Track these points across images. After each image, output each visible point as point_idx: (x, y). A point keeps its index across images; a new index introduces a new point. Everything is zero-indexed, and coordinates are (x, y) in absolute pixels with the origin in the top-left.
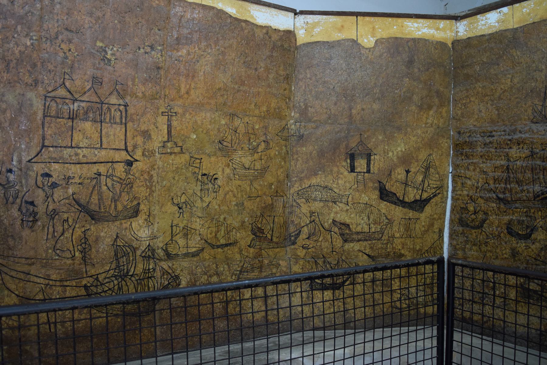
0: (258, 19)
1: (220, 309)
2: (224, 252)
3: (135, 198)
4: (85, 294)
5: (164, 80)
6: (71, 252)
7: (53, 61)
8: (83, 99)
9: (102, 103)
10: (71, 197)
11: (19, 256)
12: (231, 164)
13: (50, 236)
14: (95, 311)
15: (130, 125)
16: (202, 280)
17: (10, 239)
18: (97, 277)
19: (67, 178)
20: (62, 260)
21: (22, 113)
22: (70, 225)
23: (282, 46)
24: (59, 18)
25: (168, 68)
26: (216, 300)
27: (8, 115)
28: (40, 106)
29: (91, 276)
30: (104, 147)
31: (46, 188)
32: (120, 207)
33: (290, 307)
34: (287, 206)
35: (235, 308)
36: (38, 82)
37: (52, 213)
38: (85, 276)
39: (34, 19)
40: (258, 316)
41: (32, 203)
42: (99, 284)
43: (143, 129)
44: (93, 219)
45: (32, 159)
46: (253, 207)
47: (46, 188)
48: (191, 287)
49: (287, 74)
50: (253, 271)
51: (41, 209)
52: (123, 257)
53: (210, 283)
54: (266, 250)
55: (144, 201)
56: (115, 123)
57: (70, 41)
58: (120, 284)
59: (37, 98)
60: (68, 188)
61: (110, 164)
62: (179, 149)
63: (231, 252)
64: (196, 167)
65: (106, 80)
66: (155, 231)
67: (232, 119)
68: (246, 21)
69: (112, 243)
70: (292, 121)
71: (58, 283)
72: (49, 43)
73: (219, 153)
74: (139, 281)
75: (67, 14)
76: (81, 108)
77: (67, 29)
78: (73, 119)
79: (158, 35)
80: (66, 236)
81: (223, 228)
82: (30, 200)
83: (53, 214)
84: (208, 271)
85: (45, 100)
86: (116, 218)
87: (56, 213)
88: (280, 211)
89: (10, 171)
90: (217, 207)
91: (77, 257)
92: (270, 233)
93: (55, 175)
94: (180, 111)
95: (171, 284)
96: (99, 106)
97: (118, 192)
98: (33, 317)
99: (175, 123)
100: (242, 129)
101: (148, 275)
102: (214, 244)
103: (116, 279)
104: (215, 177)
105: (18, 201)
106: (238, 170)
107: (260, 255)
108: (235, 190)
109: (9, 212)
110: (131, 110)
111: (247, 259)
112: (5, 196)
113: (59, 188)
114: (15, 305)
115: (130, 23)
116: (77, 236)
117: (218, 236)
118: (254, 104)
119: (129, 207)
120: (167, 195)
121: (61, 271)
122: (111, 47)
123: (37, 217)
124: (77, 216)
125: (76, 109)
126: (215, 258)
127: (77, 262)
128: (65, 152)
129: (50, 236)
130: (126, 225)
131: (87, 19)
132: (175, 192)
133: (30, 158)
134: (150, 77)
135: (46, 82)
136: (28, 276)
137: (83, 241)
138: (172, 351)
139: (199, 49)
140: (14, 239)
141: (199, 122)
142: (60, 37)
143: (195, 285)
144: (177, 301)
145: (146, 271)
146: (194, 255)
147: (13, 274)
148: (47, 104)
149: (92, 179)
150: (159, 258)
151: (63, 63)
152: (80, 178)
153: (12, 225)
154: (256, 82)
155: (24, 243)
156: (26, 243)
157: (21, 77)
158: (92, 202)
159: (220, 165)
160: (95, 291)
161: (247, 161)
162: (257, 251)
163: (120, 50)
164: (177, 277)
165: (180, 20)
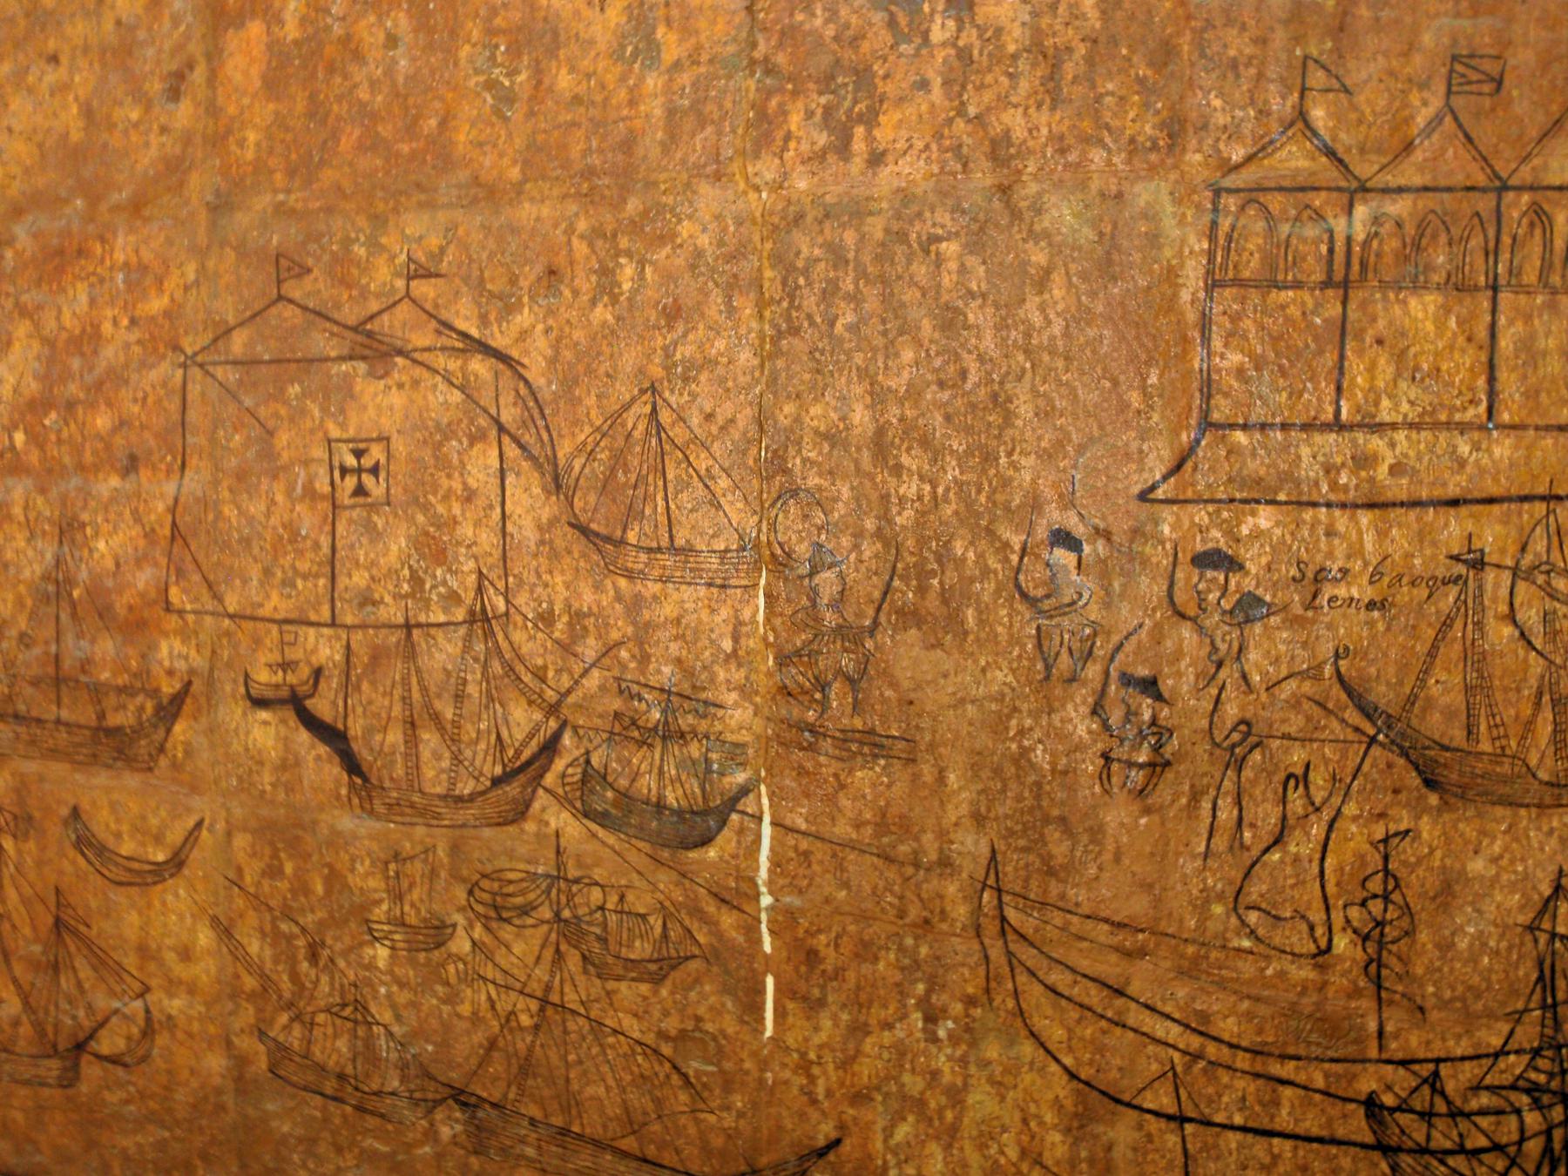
4: (1369, 1139)
6: (1312, 928)
10: (1328, 670)
11: (1085, 910)
13: (1220, 843)
17: (1053, 833)
18: (1436, 1074)
19: (1310, 575)
20: (1267, 958)
22: (1318, 801)
28: (1192, 239)
29: (1404, 1063)
36: (1183, 129)
37: (1236, 736)
38: (1373, 1053)
41: (1150, 686)
44: (1430, 783)
45: (1153, 488)
59: (1178, 202)
61: (1540, 508)
65: (1522, 58)
71: (1242, 1061)
78: (1345, 285)
80: (1293, 849)
82: (1143, 671)
87: (1252, 740)
93: (1254, 559)
96: (1485, 204)
103: (1537, 1105)
105: (1093, 671)
109: (1056, 718)
112: (1039, 645)
116: (1349, 857)
121: (1263, 1010)
124: (1351, 765)
129: (1220, 843)
136: (1119, 1002)
137: (1375, 885)
140: (1068, 831)
147: (1058, 978)
148: (1225, 224)
149: (1437, 584)
153: (1065, 773)
155: (1107, 857)
156: (1117, 859)
157: (1107, 117)
158: (1429, 699)
160: (1420, 1137)
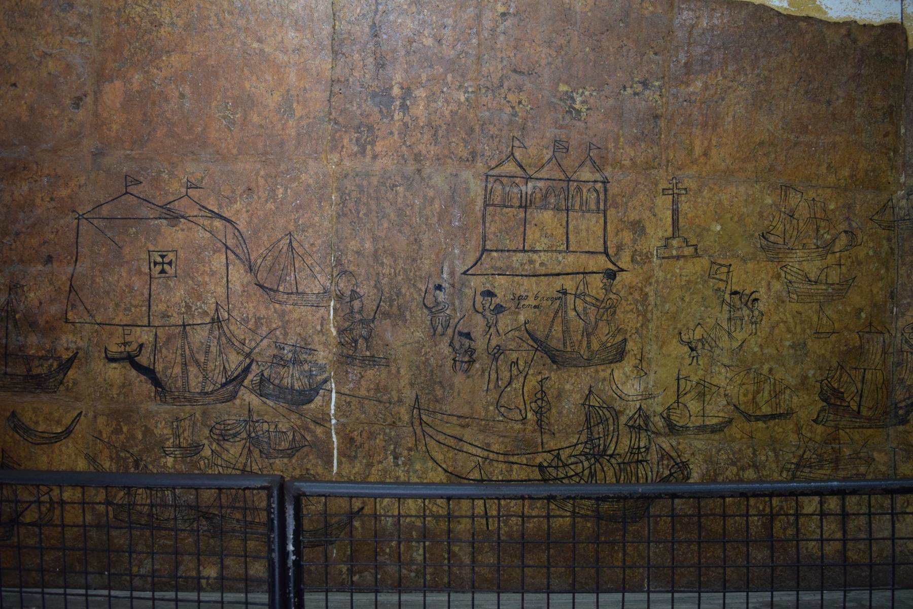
0: (829, 11)
1: (757, 527)
2: (768, 428)
3: (619, 331)
4: (540, 478)
5: (666, 136)
7: (496, 122)
8: (541, 176)
9: (569, 180)
10: (523, 328)
11: (449, 413)
12: (783, 275)
14: (554, 506)
15: (611, 212)
16: (728, 473)
21: (455, 202)
23: (879, 54)
24: (504, 55)
25: (673, 115)
26: (752, 511)
27: (437, 206)
28: (479, 191)
29: (549, 452)
30: (571, 249)
31: (487, 313)
32: (595, 345)
33: (893, 538)
34: (891, 350)
35: (785, 529)
38: (540, 450)
39: (469, 61)
40: (829, 548)
41: (468, 336)
42: (561, 464)
43: (632, 218)
44: (554, 362)
45: (468, 270)
46: (823, 352)
47: (487, 313)
48: (708, 483)
49: (891, 106)
50: (821, 467)
51: (480, 344)
52: (598, 424)
53: (741, 481)
54: (848, 431)
55: (634, 337)
56: (589, 211)
57: (520, 89)
58: (593, 467)
60: (519, 313)
61: (581, 276)
62: (691, 249)
63: (781, 430)
64: (721, 280)
65: (573, 143)
66: (650, 386)
67: (786, 195)
68: (807, 19)
69: (581, 402)
70: (901, 193)
71: (501, 458)
72: (490, 94)
73: (761, 255)
74: (622, 466)
75: (515, 48)
76: (537, 190)
77: (515, 71)
78: (526, 207)
79: (653, 62)
81: (767, 387)
82: (466, 331)
83: (497, 353)
84: (738, 460)
85: (487, 181)
86: (588, 363)
88: (877, 360)
89: (439, 287)
90: (756, 349)
91: (530, 420)
92: (857, 399)
94: (693, 185)
95: (675, 475)
96: (564, 185)
97: (593, 320)
98: (465, 504)
99: (684, 207)
100: (803, 212)
101: (637, 457)
102: (750, 412)
103: (587, 459)
104: (753, 296)
105: (450, 331)
106: (796, 285)
107: (836, 439)
108: (790, 320)
109: (437, 348)
110: (613, 189)
111: (810, 444)
113: (506, 313)
114: (441, 484)
115: (608, 49)
117: (757, 400)
118: (825, 165)
119: (609, 344)
120: (671, 327)
121: (507, 440)
122: (581, 91)
123: (474, 356)
125: (529, 192)
126: (752, 437)
127: (529, 427)
128: (514, 259)
129: (492, 386)
130: (604, 373)
131: (545, 51)
132: (684, 322)
133: (467, 268)
134: (643, 133)
135: (488, 153)
136: (461, 443)
138: (673, 587)
139: (725, 78)
141: (726, 203)
142: (506, 84)
143: (714, 481)
144: (683, 504)
145: (634, 450)
146: (715, 430)
147: (441, 438)
149: (553, 300)
150: (655, 430)
151: (511, 123)
152: (536, 297)
154: (830, 125)
155: (455, 394)
157: (453, 149)
159: (763, 275)
161: (812, 269)
162: (829, 431)
163: (594, 94)
164: (685, 465)
165: (690, 33)
